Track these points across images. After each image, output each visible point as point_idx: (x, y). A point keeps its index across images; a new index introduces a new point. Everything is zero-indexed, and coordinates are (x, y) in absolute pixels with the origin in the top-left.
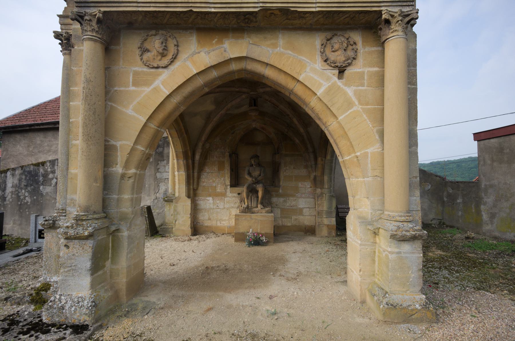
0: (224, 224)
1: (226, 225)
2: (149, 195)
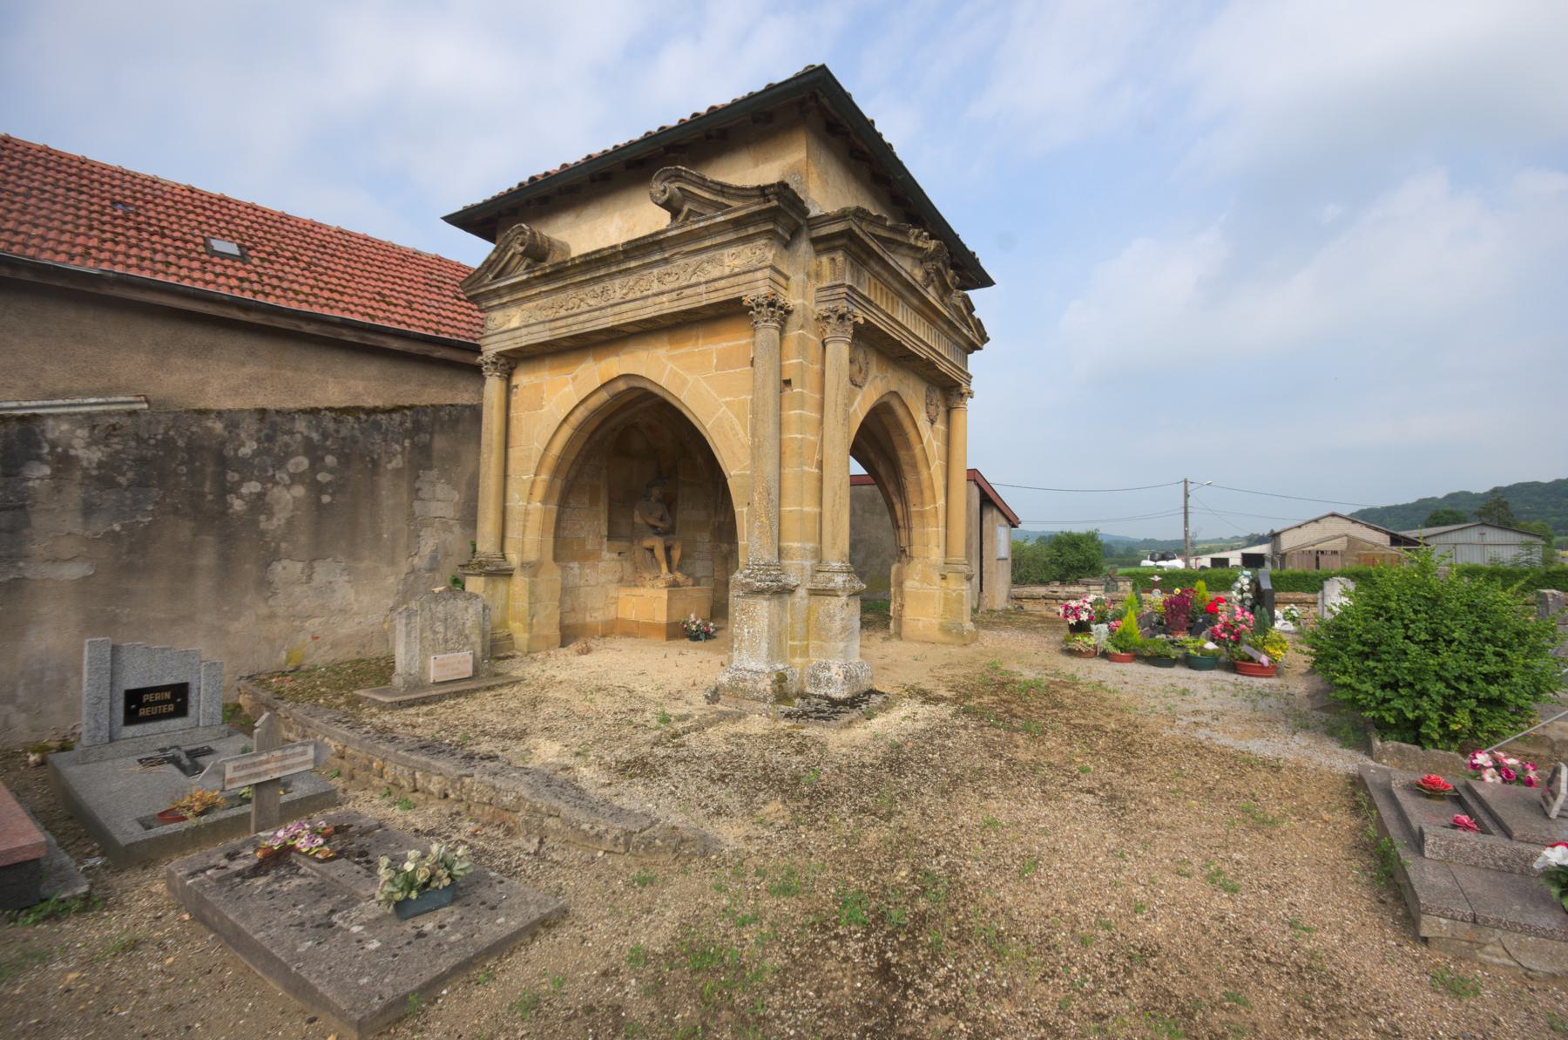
2: (392, 562)
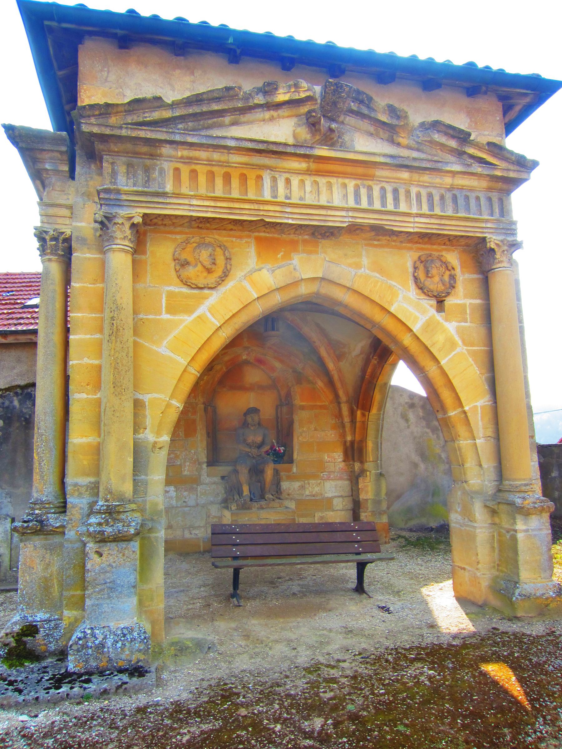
0: (196, 534)
1: (200, 535)
